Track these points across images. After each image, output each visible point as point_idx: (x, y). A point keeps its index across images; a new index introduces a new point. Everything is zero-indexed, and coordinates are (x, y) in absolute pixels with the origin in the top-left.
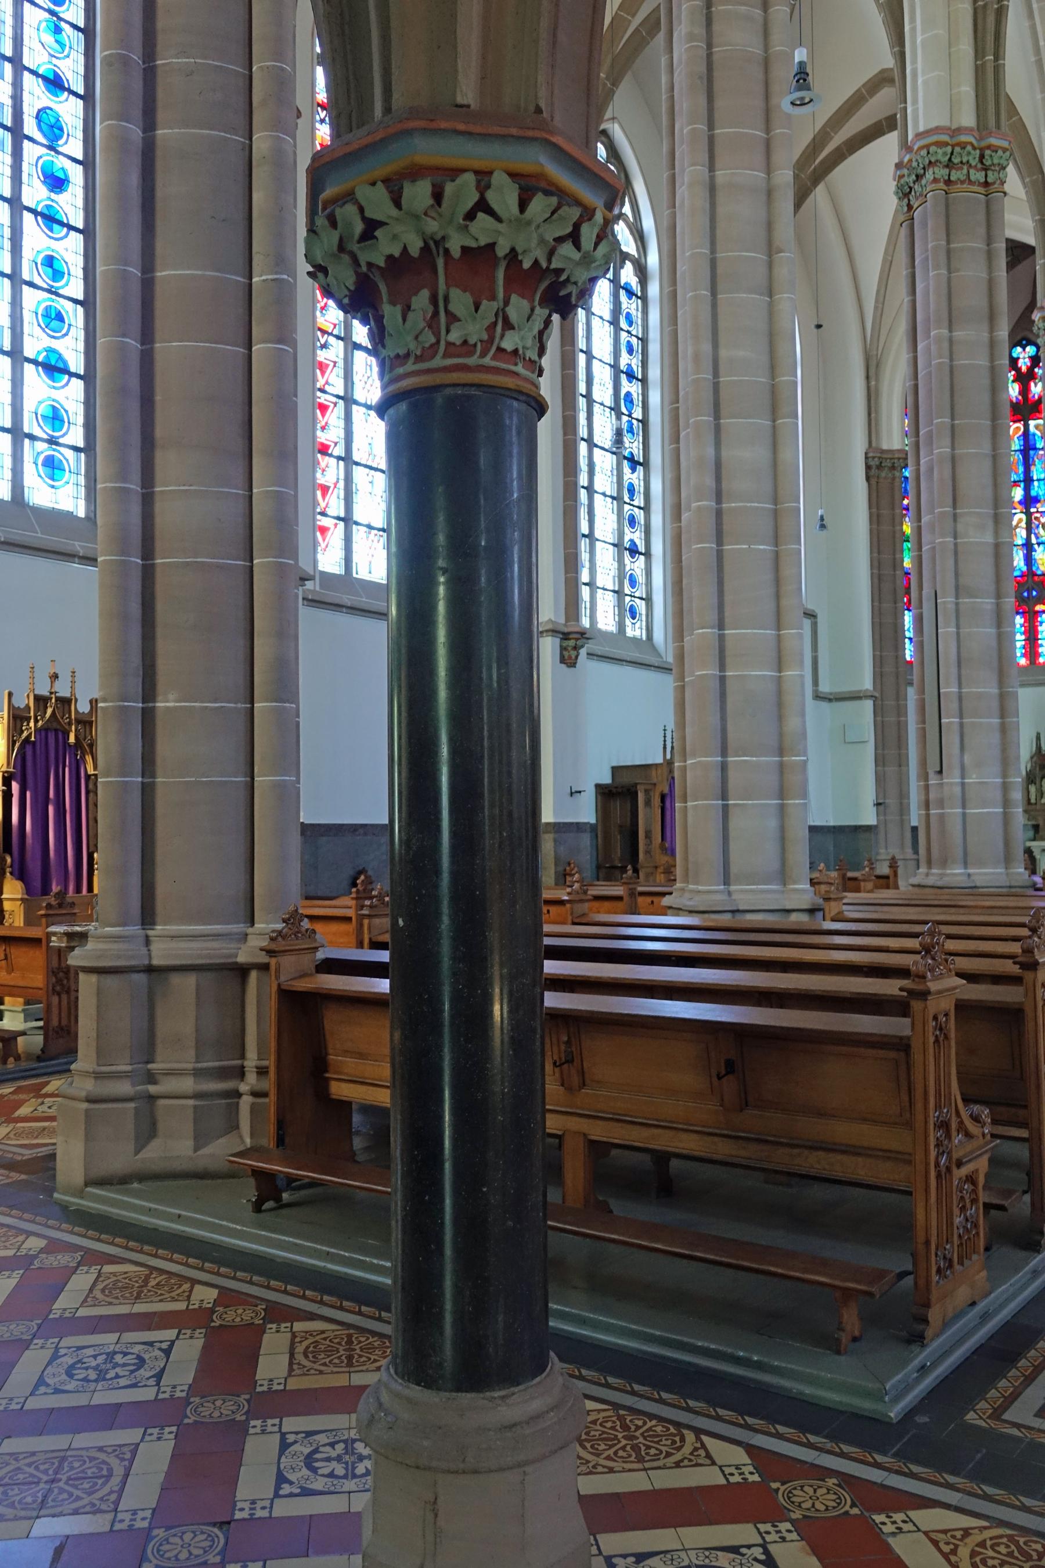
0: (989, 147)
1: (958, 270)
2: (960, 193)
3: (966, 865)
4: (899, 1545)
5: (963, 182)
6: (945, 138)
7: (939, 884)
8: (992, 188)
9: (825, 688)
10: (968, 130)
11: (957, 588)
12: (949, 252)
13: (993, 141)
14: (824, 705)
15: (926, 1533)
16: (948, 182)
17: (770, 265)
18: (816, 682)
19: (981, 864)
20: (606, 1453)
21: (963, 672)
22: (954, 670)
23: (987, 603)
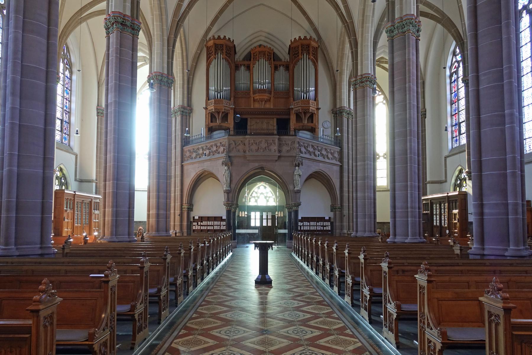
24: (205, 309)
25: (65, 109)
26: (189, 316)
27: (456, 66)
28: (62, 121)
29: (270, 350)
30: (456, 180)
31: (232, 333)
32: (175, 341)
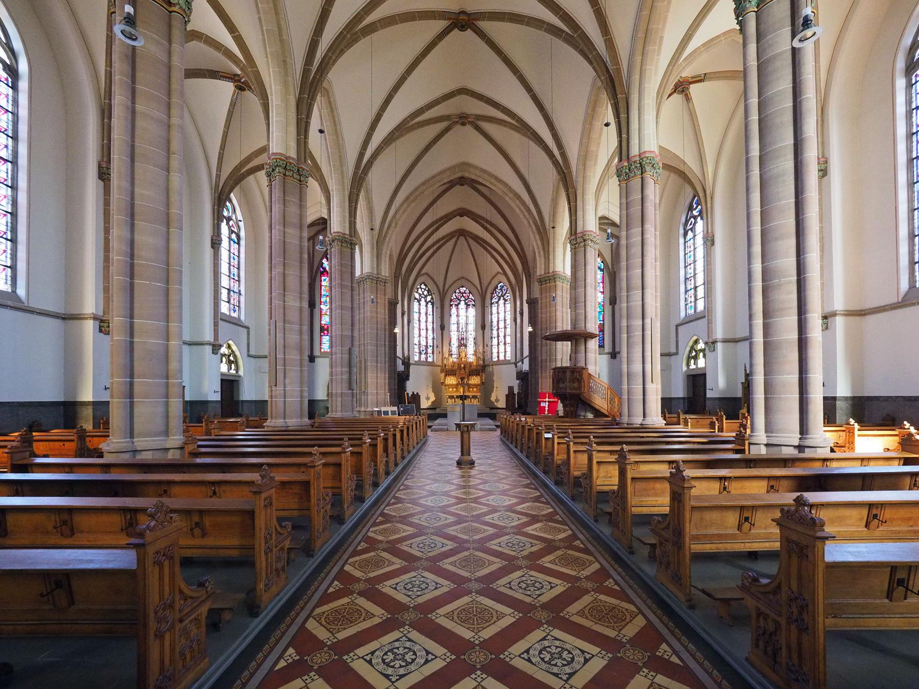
0: (301, 168)
1: (287, 207)
2: (289, 180)
3: (285, 418)
4: (438, 621)
7: (274, 426)
9: (252, 352)
10: (293, 159)
11: (284, 320)
14: (252, 359)
15: (444, 616)
16: (285, 175)
18: (248, 351)
19: (291, 418)
20: (339, 624)
21: (286, 350)
22: (282, 349)
23: (297, 327)
24: (404, 494)
25: (232, 277)
26: (351, 549)
27: (692, 222)
28: (229, 290)
29: (476, 577)
30: (690, 352)
31: (427, 543)
32: (351, 560)
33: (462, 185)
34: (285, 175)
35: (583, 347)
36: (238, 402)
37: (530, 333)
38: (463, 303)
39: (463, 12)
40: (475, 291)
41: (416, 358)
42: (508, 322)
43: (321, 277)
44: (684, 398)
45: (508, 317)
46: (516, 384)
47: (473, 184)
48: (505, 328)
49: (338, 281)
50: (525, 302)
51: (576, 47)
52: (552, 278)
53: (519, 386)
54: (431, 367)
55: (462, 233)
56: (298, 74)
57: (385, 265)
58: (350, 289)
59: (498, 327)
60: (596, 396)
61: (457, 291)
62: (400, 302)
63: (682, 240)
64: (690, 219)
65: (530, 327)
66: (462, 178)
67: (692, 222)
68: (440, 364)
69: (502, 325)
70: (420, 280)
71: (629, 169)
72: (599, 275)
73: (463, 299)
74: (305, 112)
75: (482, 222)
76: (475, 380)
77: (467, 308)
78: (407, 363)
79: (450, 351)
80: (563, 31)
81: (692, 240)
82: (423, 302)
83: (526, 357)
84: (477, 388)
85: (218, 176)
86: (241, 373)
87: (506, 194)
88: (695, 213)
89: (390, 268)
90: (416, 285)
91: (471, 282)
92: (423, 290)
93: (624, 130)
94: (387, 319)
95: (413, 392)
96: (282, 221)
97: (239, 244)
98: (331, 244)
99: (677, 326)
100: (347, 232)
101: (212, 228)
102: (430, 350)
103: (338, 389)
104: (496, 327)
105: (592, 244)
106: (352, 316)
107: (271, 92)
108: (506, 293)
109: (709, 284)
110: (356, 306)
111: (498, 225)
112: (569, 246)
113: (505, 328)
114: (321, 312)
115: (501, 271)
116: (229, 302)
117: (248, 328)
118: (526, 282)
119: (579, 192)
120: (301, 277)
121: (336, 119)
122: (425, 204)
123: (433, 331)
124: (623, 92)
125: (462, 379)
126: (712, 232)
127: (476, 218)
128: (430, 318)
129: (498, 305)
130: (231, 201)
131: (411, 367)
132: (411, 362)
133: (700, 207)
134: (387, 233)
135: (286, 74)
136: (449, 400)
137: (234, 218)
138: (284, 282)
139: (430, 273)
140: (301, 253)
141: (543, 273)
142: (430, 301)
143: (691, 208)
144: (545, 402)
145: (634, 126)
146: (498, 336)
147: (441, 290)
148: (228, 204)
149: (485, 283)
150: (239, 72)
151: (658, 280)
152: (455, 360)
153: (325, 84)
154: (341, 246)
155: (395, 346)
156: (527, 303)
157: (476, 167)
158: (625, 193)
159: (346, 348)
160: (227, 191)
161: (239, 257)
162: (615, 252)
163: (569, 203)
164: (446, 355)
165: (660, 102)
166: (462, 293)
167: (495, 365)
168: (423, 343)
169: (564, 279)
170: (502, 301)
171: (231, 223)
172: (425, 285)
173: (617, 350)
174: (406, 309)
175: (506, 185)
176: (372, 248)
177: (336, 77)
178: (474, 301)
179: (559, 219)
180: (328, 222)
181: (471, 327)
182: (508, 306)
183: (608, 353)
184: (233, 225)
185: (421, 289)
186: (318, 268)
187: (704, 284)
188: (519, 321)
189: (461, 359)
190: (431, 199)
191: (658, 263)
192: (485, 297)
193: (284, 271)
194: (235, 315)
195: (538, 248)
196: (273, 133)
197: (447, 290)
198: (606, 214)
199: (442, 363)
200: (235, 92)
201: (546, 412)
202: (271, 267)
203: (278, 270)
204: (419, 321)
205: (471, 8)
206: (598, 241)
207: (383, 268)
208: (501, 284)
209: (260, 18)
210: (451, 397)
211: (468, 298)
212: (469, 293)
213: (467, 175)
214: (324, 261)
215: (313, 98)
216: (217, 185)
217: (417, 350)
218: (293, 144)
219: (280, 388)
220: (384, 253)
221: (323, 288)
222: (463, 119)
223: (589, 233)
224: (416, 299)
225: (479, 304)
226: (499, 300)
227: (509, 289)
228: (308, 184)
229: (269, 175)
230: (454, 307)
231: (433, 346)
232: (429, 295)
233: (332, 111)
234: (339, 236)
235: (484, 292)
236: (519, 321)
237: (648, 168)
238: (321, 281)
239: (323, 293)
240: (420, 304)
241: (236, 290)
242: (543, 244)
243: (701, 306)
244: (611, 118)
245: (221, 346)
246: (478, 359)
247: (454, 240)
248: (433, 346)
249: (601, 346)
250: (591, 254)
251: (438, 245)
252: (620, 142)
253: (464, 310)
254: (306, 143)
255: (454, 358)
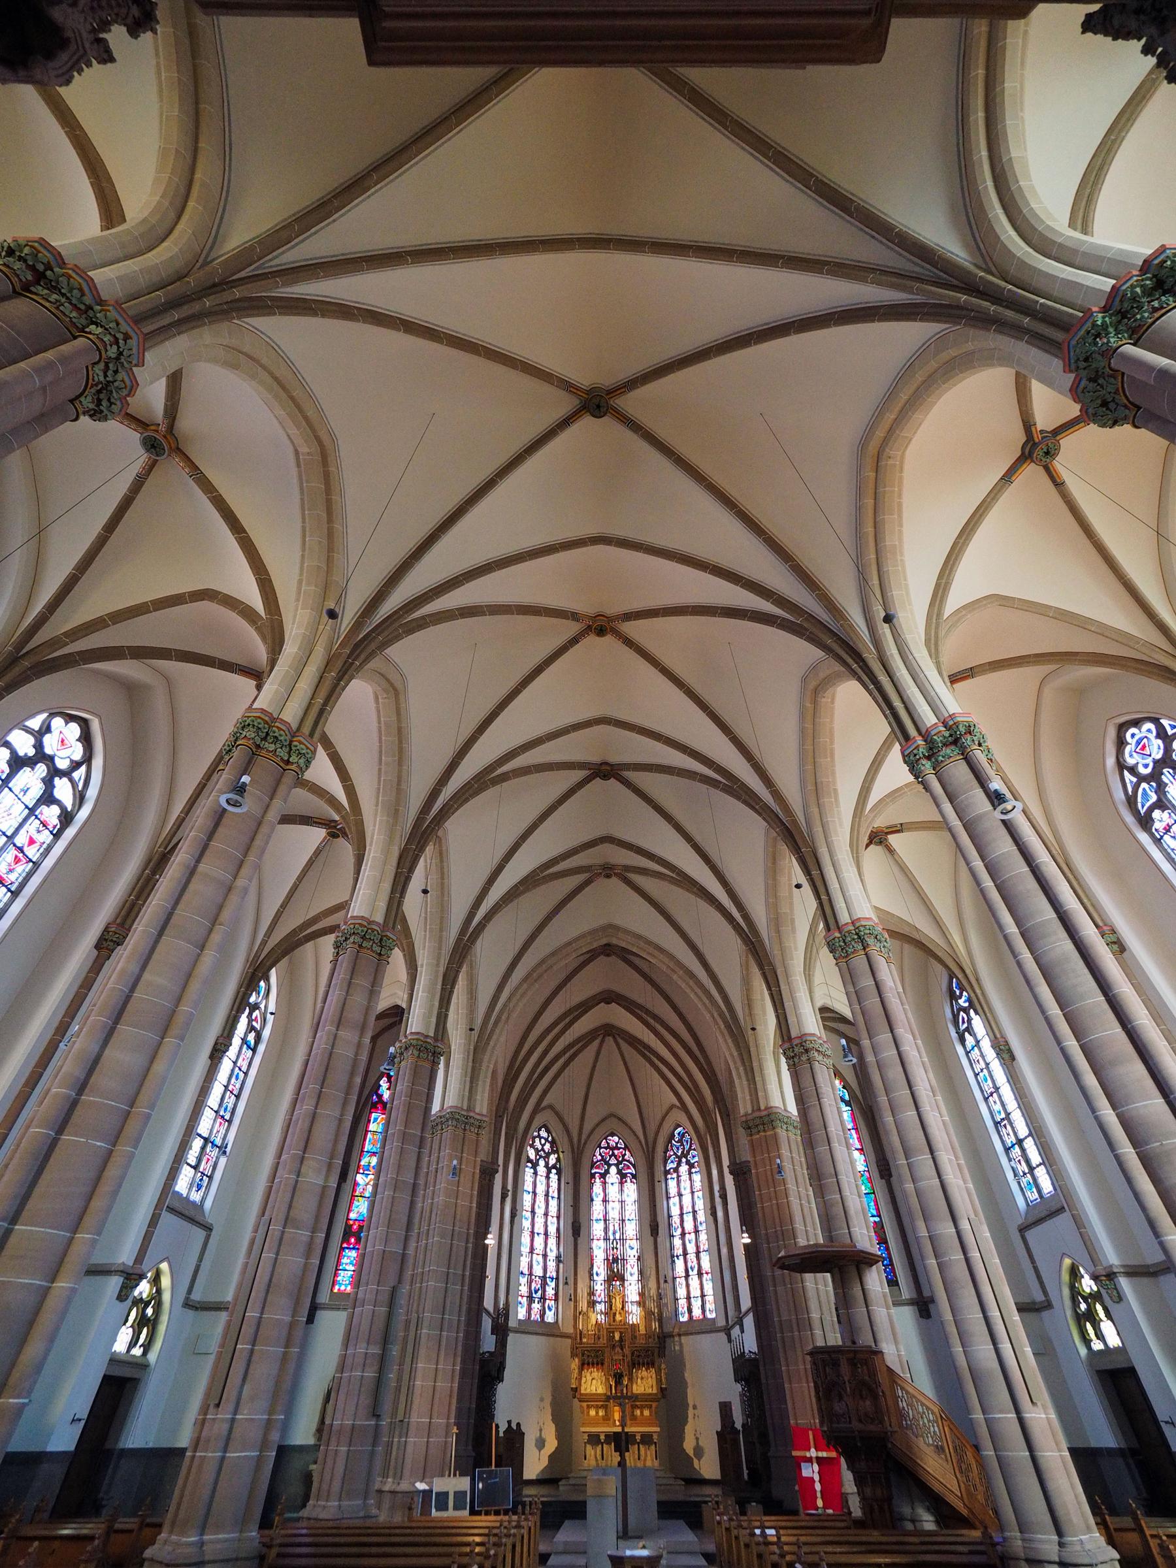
0: (386, 936)
2: (366, 955)
5: (368, 949)
6: (365, 923)
8: (382, 958)
10: (378, 924)
12: (350, 983)
13: (388, 934)
16: (360, 946)
17: (211, 931)
27: (963, 1019)
33: (608, 955)
34: (360, 946)
35: (857, 1291)
36: (110, 1452)
37: (746, 1246)
38: (613, 1170)
39: (606, 763)
40: (633, 1144)
41: (522, 1313)
42: (701, 1217)
43: (371, 1113)
44: (1120, 1452)
45: (700, 1205)
46: (733, 1392)
47: (625, 955)
48: (697, 1231)
49: (400, 1127)
50: (726, 1171)
51: (738, 798)
52: (766, 1120)
53: (742, 1402)
54: (552, 1339)
55: (608, 1031)
56: (410, 821)
57: (483, 1092)
58: (418, 1143)
59: (683, 1229)
60: (920, 1442)
61: (604, 1144)
62: (501, 1169)
63: (960, 1050)
64: (959, 1014)
65: (745, 1235)
66: (608, 945)
67: (963, 1019)
68: (571, 1331)
69: (689, 1225)
70: (537, 1122)
71: (844, 941)
72: (846, 1110)
73: (613, 1161)
74: (407, 865)
75: (639, 1012)
76: (645, 1383)
77: (621, 1183)
78: (501, 1330)
79: (592, 1293)
80: (721, 782)
81: (976, 1048)
82: (541, 1169)
83: (747, 1313)
84: (650, 1407)
85: (264, 943)
86: (152, 1357)
87: (673, 970)
88: (962, 1002)
89: (490, 1104)
90: (530, 1132)
91: (627, 1125)
92: (543, 1141)
93: (822, 890)
94: (474, 1209)
95: (509, 1422)
96: (336, 1019)
97: (254, 1050)
98: (402, 1054)
99: (1023, 1230)
100: (432, 1034)
101: (225, 1020)
102: (550, 1291)
103: (345, 1417)
104: (679, 1231)
105: (820, 1058)
106: (412, 1204)
107: (372, 842)
108: (690, 1149)
109: (1037, 1131)
110: (421, 1182)
111: (665, 1018)
112: (783, 1060)
113: (697, 1231)
114: (354, 1190)
115: (678, 1104)
116: (196, 1168)
117: (208, 1229)
118: (723, 1125)
119: (780, 972)
120: (340, 1121)
121: (445, 870)
122: (553, 984)
123: (558, 1237)
124: (807, 846)
125: (618, 1378)
126: (1002, 1037)
127: (631, 1006)
128: (553, 1204)
129: (678, 1176)
130: (267, 980)
131: (511, 1338)
132: (512, 1323)
133: (965, 993)
134: (492, 1031)
135: (395, 824)
136: (589, 1447)
137: (262, 1006)
138: (310, 1131)
139: (558, 1107)
140: (352, 1074)
141: (750, 1112)
142: (554, 1167)
143: (953, 997)
144: (810, 1460)
145: (833, 885)
146: (685, 1254)
147: (575, 1140)
148: (262, 984)
149: (652, 1127)
150: (337, 818)
151: (952, 1131)
152: (601, 1318)
153: (440, 833)
154: (418, 1057)
155: (483, 1277)
156: (731, 1173)
157: (627, 932)
158: (849, 977)
159: (386, 1289)
160: (268, 963)
161: (246, 1074)
162: (861, 1070)
163: (769, 988)
164: (583, 1305)
165: (858, 857)
166: (613, 1149)
167: (687, 1334)
168: (538, 1271)
169: (787, 1121)
170: (684, 1168)
171: (256, 1013)
172: (548, 1131)
173: (926, 1293)
174: (510, 1187)
175: (672, 957)
176: (466, 1059)
177: (456, 829)
178: (634, 1166)
179: (757, 1011)
180: (406, 1015)
181: (631, 1229)
182: (697, 1178)
183: (911, 1302)
184: (256, 1017)
185: (543, 1145)
186: (370, 1096)
187: (1030, 1134)
188: (720, 1214)
189: (615, 1314)
190: (563, 976)
191: (939, 1098)
192: (653, 1158)
193: (316, 1108)
194: (196, 1197)
195: (735, 1063)
196: (359, 890)
197: (585, 1144)
198: (829, 1003)
199: (575, 1326)
200: (325, 838)
201: (820, 1503)
202: (297, 1099)
203: (306, 1107)
204: (533, 1212)
205: (614, 759)
206: (829, 1053)
207: (478, 1097)
208: (679, 1129)
209: (380, 770)
210: (594, 1439)
211: (624, 1160)
212: (624, 1149)
213: (614, 941)
214: (384, 1084)
215: (421, 849)
216: (257, 955)
217: (524, 1290)
218: (382, 905)
219: (224, 1415)
220: (484, 1068)
221: (369, 1135)
222: (608, 871)
223: (811, 1038)
224: (530, 1161)
225: (643, 1176)
226: (679, 1164)
227: (695, 1140)
228: (390, 960)
229: (337, 946)
230: (598, 1180)
231: (557, 1279)
232: (553, 1152)
233: (442, 861)
234: (417, 1039)
235: (650, 1145)
236: (720, 1214)
237: (871, 941)
238: (369, 1121)
239: (367, 1147)
240: (536, 1173)
241: (218, 1142)
242: (741, 1055)
243: (1047, 1186)
244: (801, 878)
245: (142, 1277)
246: (648, 1315)
247: (596, 1043)
248: (557, 1279)
249: (893, 1282)
250: (823, 1075)
251: (572, 1051)
252: (821, 904)
253: (616, 1187)
254: (400, 904)
255: (598, 1316)
